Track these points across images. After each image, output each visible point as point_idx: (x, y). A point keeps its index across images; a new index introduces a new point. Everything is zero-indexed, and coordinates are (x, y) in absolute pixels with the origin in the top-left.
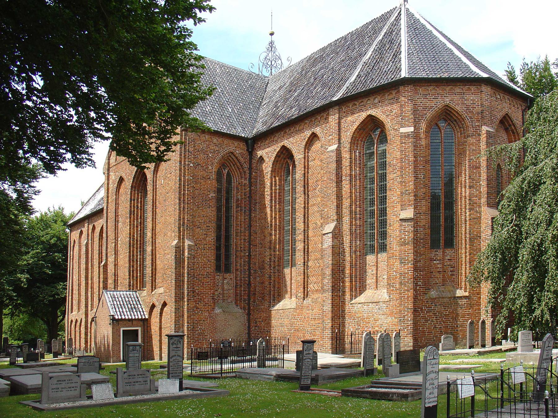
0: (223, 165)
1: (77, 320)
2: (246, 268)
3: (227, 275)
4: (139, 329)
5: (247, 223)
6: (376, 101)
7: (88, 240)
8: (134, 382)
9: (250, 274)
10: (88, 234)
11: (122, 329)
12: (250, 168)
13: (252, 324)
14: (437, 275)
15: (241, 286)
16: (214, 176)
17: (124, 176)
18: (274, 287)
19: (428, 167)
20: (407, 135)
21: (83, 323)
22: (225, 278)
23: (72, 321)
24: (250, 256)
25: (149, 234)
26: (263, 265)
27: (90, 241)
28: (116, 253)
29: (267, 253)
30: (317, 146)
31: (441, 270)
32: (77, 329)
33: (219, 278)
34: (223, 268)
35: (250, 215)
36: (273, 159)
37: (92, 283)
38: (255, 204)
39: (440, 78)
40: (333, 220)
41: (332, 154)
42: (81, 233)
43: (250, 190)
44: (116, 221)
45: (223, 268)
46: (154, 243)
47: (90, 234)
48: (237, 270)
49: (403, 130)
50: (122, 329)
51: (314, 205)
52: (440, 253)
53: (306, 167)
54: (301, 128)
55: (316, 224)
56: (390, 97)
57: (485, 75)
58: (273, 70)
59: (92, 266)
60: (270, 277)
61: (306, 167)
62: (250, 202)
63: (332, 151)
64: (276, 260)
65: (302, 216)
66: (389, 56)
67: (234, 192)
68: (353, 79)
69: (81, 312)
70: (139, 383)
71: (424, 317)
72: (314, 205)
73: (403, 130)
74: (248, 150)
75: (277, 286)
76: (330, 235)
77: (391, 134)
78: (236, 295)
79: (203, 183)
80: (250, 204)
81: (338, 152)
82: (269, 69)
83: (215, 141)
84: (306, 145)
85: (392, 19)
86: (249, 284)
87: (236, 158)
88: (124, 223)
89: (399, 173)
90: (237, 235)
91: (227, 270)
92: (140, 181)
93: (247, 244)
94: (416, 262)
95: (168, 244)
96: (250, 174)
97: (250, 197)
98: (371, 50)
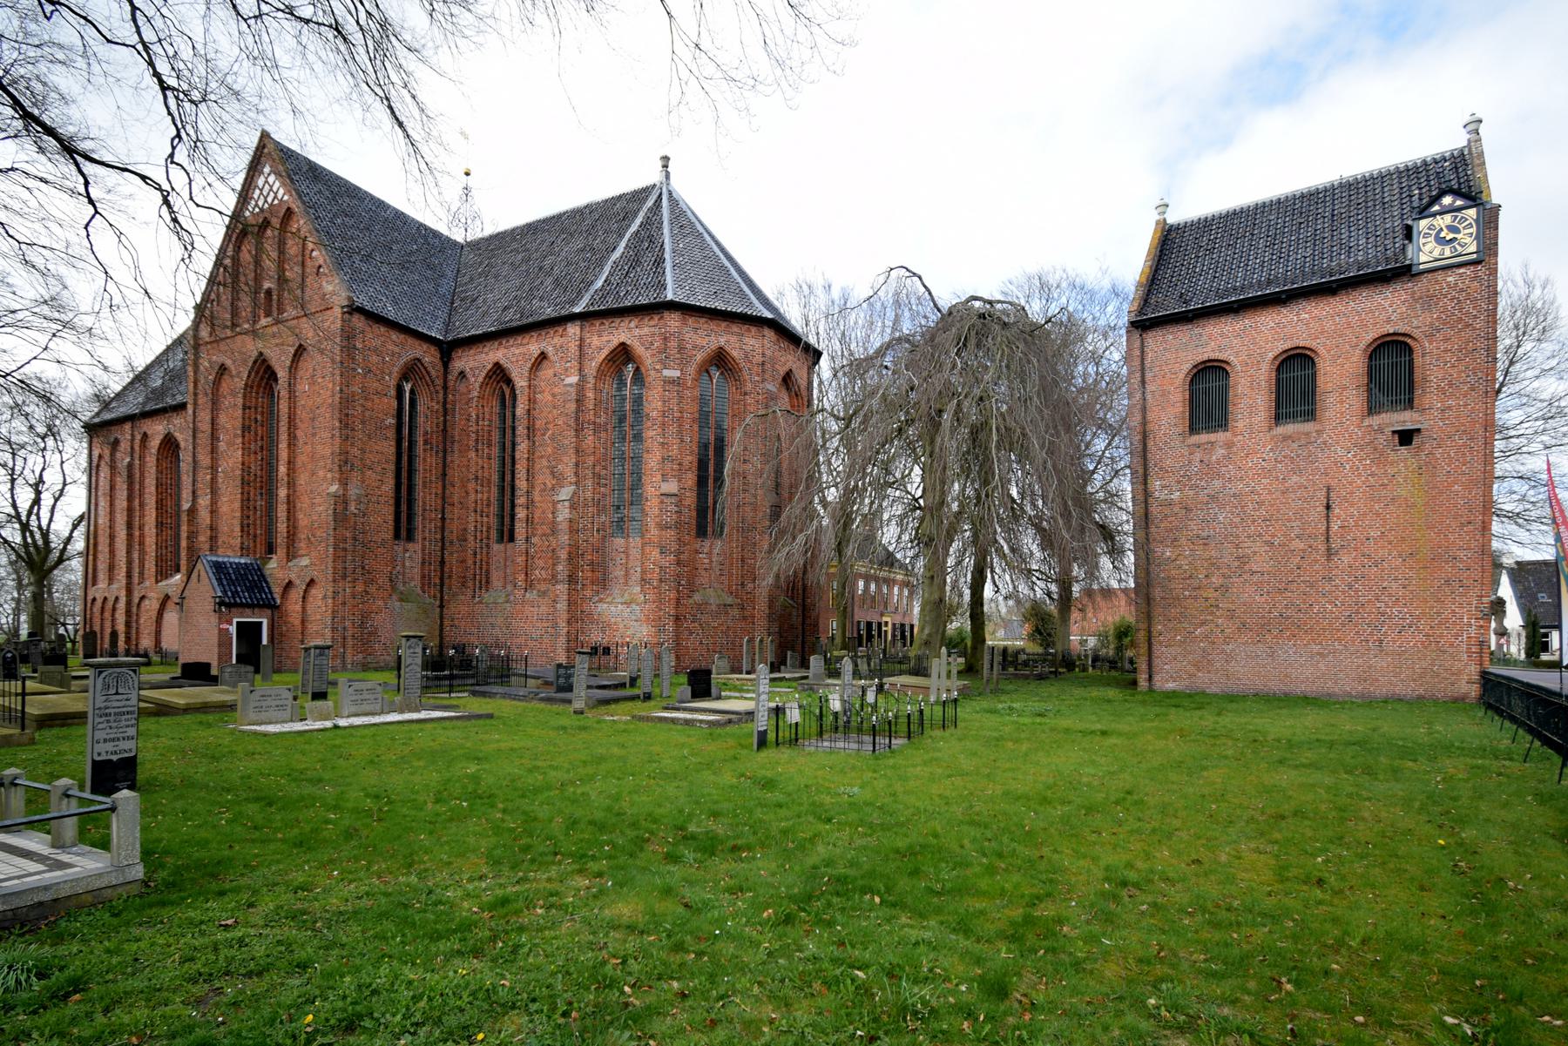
0: (405, 376)
2: (439, 536)
3: (410, 546)
5: (440, 470)
6: (632, 325)
7: (132, 459)
9: (443, 548)
10: (132, 448)
11: (235, 620)
12: (445, 388)
13: (446, 622)
14: (703, 573)
16: (393, 392)
19: (696, 428)
20: (672, 381)
21: (122, 605)
23: (94, 599)
24: (443, 519)
25: (283, 469)
26: (463, 535)
28: (214, 491)
29: (471, 519)
30: (546, 372)
32: (107, 615)
34: (403, 533)
35: (445, 458)
36: (480, 379)
37: (142, 536)
38: (453, 443)
39: (715, 309)
41: (572, 390)
43: (445, 421)
44: (214, 437)
45: (403, 533)
46: (291, 484)
47: (137, 448)
49: (666, 373)
50: (235, 620)
51: (542, 457)
52: (707, 543)
53: (532, 401)
54: (525, 341)
55: (545, 484)
56: (652, 323)
57: (770, 316)
59: (142, 505)
60: (475, 554)
61: (532, 401)
62: (445, 438)
63: (571, 385)
65: (524, 471)
66: (649, 259)
68: (599, 283)
69: (115, 586)
71: (688, 629)
72: (542, 457)
73: (666, 373)
74: (441, 359)
75: (484, 567)
76: (567, 504)
77: (650, 375)
78: (423, 577)
79: (377, 401)
80: (445, 443)
81: (580, 387)
83: (394, 337)
85: (650, 203)
86: (442, 562)
88: (230, 444)
89: (660, 430)
90: (424, 487)
91: (410, 538)
92: (262, 379)
93: (439, 502)
94: (678, 553)
95: (320, 490)
96: (445, 394)
97: (445, 430)
98: (623, 244)
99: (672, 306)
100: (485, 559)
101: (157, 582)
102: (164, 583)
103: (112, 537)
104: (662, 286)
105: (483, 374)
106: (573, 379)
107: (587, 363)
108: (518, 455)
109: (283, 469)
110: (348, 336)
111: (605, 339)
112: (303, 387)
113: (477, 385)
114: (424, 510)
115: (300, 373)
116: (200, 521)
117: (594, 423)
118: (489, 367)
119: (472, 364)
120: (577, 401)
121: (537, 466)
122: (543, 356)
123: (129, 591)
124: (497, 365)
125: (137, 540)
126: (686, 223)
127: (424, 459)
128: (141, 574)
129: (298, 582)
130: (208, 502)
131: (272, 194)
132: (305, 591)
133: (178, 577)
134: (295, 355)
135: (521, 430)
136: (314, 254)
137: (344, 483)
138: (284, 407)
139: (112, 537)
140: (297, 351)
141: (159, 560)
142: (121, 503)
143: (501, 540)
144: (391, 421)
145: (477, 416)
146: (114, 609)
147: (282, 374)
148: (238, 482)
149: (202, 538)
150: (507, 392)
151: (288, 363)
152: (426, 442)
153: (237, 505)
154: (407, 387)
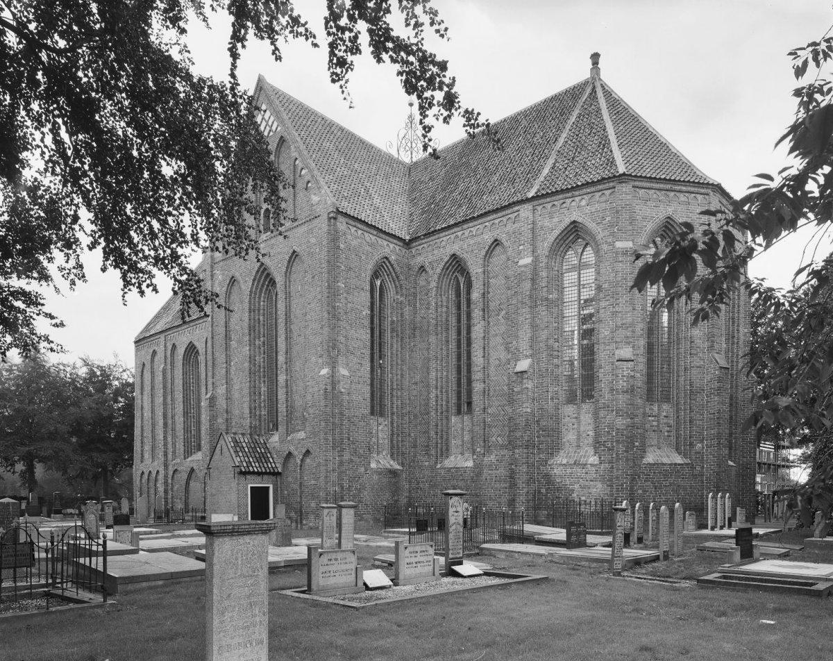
0: (376, 275)
1: (150, 472)
4: (271, 487)
8: (416, 563)
10: (165, 357)
15: (398, 435)
16: (368, 287)
17: (237, 275)
18: (442, 438)
21: (161, 477)
22: (379, 424)
27: (169, 367)
30: (498, 259)
31: (656, 429)
32: (152, 484)
33: (373, 421)
36: (439, 271)
37: (174, 423)
40: (527, 356)
42: (154, 353)
48: (393, 414)
49: (619, 244)
50: (249, 486)
53: (486, 285)
55: (499, 360)
58: (414, 154)
60: (437, 425)
61: (486, 285)
63: (525, 266)
64: (444, 403)
67: (388, 311)
68: (546, 171)
69: (156, 463)
70: (422, 564)
73: (619, 244)
75: (445, 437)
78: (392, 448)
82: (409, 152)
84: (486, 256)
85: (588, 90)
87: (392, 266)
88: (239, 342)
99: (623, 178)
100: (445, 429)
101: (185, 459)
102: (190, 459)
103: (153, 425)
104: (612, 162)
105: (441, 266)
106: (527, 260)
107: (539, 244)
108: (473, 335)
109: (281, 358)
110: (334, 238)
111: (554, 220)
112: (296, 287)
113: (436, 277)
114: (392, 389)
115: (294, 276)
116: (218, 407)
117: (547, 299)
118: (446, 259)
119: (431, 258)
120: (532, 279)
121: (492, 344)
122: (497, 243)
123: (166, 466)
124: (454, 256)
125: (170, 427)
126: (620, 110)
127: (392, 345)
128: (174, 452)
129: (295, 453)
130: (224, 392)
131: (268, 128)
132: (302, 460)
133: (200, 454)
134: (289, 262)
135: (477, 313)
136: (303, 172)
137: (333, 366)
138: (281, 306)
139: (153, 425)
140: (291, 258)
141: (187, 442)
142: (159, 400)
143: (459, 412)
144: (367, 312)
145: (436, 303)
146: (156, 480)
147: (279, 279)
148: (247, 373)
149: (220, 420)
150: (462, 280)
151: (284, 269)
152: (393, 330)
153: (246, 391)
154: (378, 283)
